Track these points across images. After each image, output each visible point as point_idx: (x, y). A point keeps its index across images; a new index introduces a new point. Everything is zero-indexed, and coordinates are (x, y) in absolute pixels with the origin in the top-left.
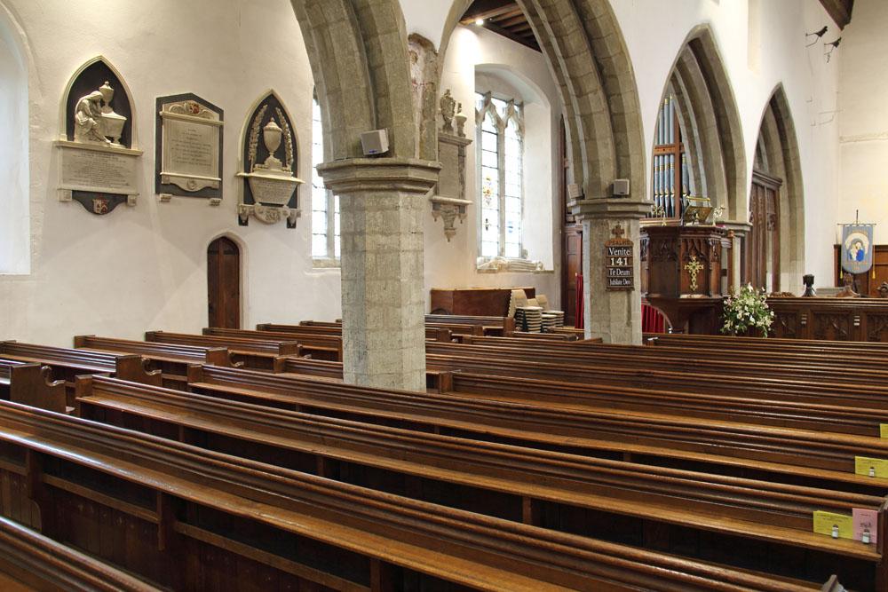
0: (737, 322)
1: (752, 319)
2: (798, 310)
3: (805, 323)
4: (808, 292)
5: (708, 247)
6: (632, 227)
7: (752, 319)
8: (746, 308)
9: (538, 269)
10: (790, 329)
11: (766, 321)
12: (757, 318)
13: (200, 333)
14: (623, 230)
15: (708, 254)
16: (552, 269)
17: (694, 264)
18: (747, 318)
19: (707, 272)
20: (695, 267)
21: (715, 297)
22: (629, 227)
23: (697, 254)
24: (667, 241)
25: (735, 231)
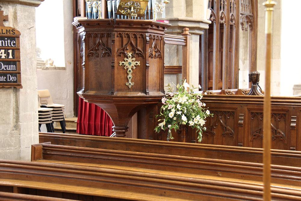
0: (170, 121)
1: (184, 118)
2: (236, 109)
3: (294, 125)
4: (253, 89)
5: (145, 42)
6: (19, 14)
7: (184, 118)
8: (178, 106)
9: (48, 66)
10: (228, 127)
11: (199, 121)
12: (189, 118)
13: (26, 156)
14: (7, 16)
15: (144, 49)
16: (64, 66)
17: (130, 60)
18: (179, 117)
19: (144, 69)
20: (131, 62)
21: (152, 93)
22: (15, 13)
23: (134, 49)
24: (102, 36)
25: (191, 28)
